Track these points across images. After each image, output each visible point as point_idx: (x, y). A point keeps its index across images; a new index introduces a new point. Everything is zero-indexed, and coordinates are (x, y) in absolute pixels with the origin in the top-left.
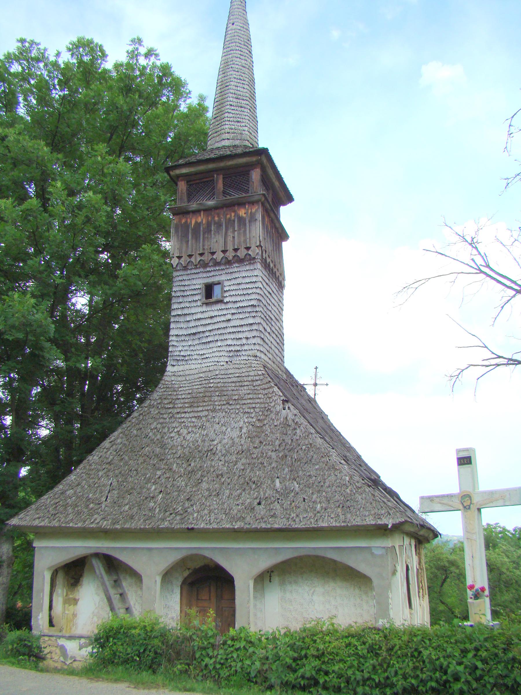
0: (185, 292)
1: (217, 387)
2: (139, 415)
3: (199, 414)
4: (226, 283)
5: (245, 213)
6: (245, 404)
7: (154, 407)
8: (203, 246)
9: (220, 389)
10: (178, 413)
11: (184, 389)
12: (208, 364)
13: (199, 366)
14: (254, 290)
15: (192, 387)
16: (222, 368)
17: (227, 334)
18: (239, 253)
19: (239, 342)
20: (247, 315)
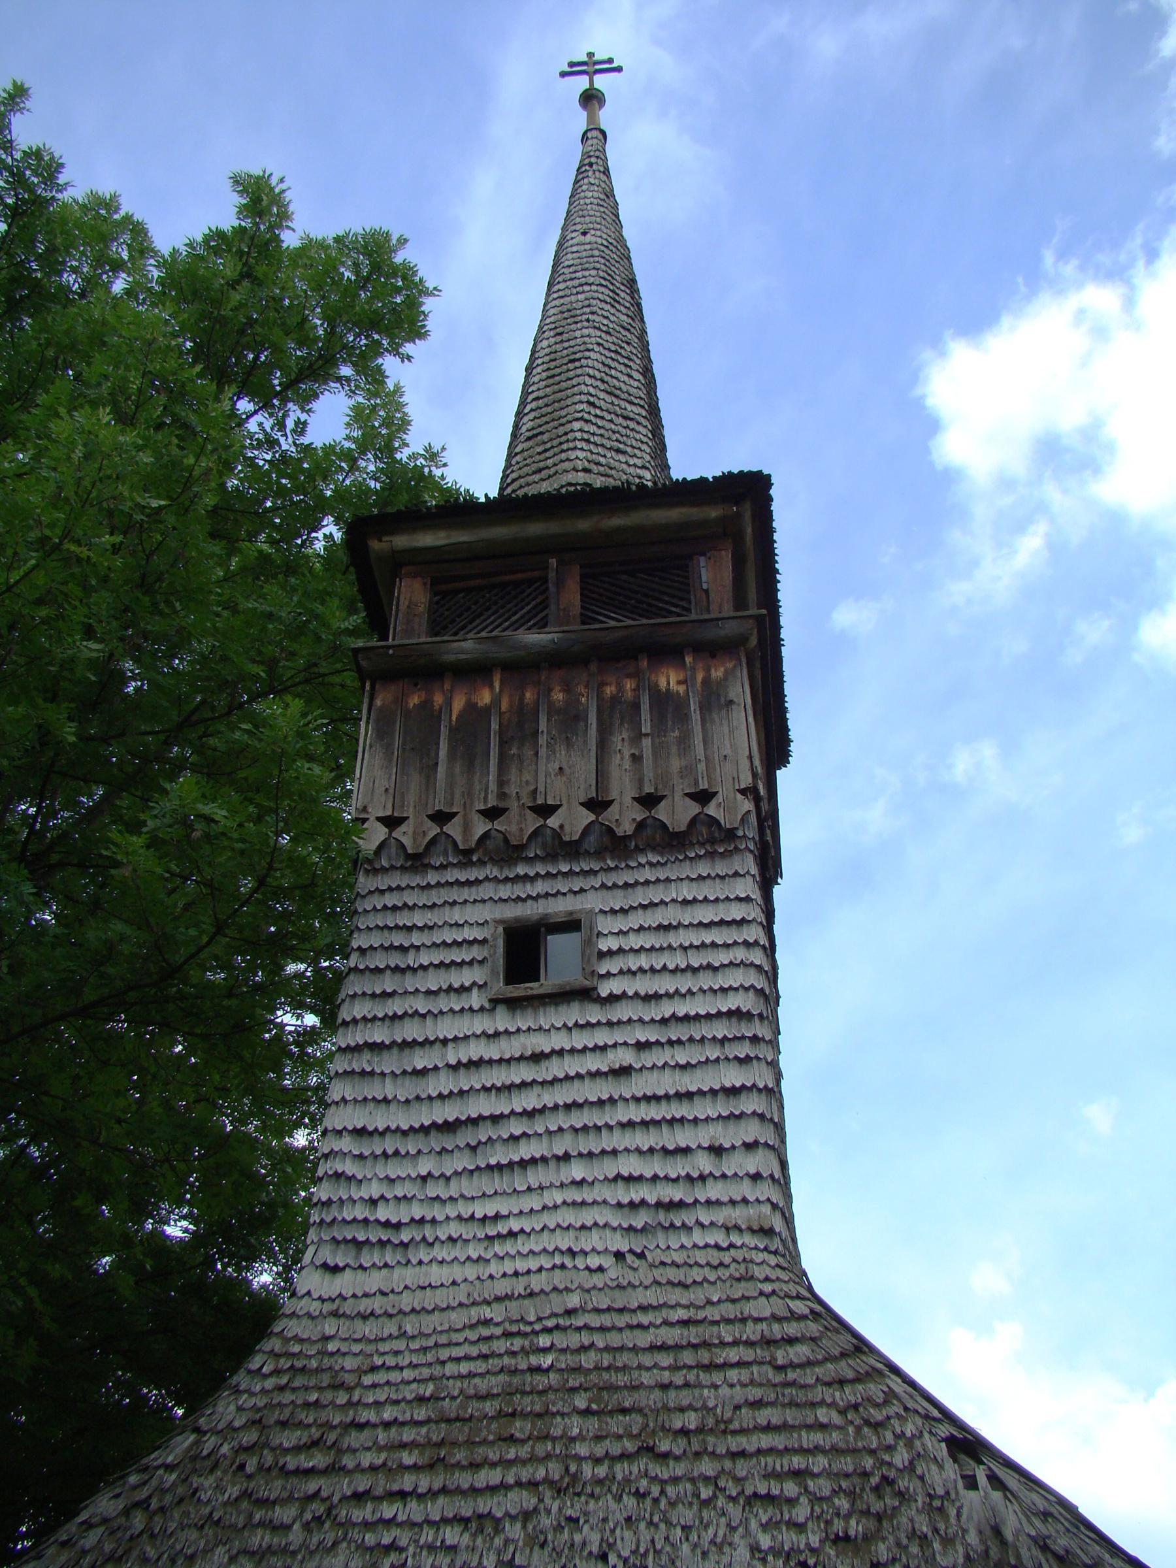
0: (412, 953)
1: (578, 1369)
2: (127, 1512)
3: (484, 1505)
4: (605, 924)
5: (679, 683)
6: (742, 1454)
7: (215, 1466)
8: (501, 783)
9: (594, 1377)
10: (359, 1497)
11: (394, 1376)
12: (521, 1266)
13: (471, 1272)
14: (740, 954)
15: (437, 1370)
16: (598, 1280)
17: (617, 1132)
18: (662, 813)
19: (677, 1168)
20: (713, 1053)
